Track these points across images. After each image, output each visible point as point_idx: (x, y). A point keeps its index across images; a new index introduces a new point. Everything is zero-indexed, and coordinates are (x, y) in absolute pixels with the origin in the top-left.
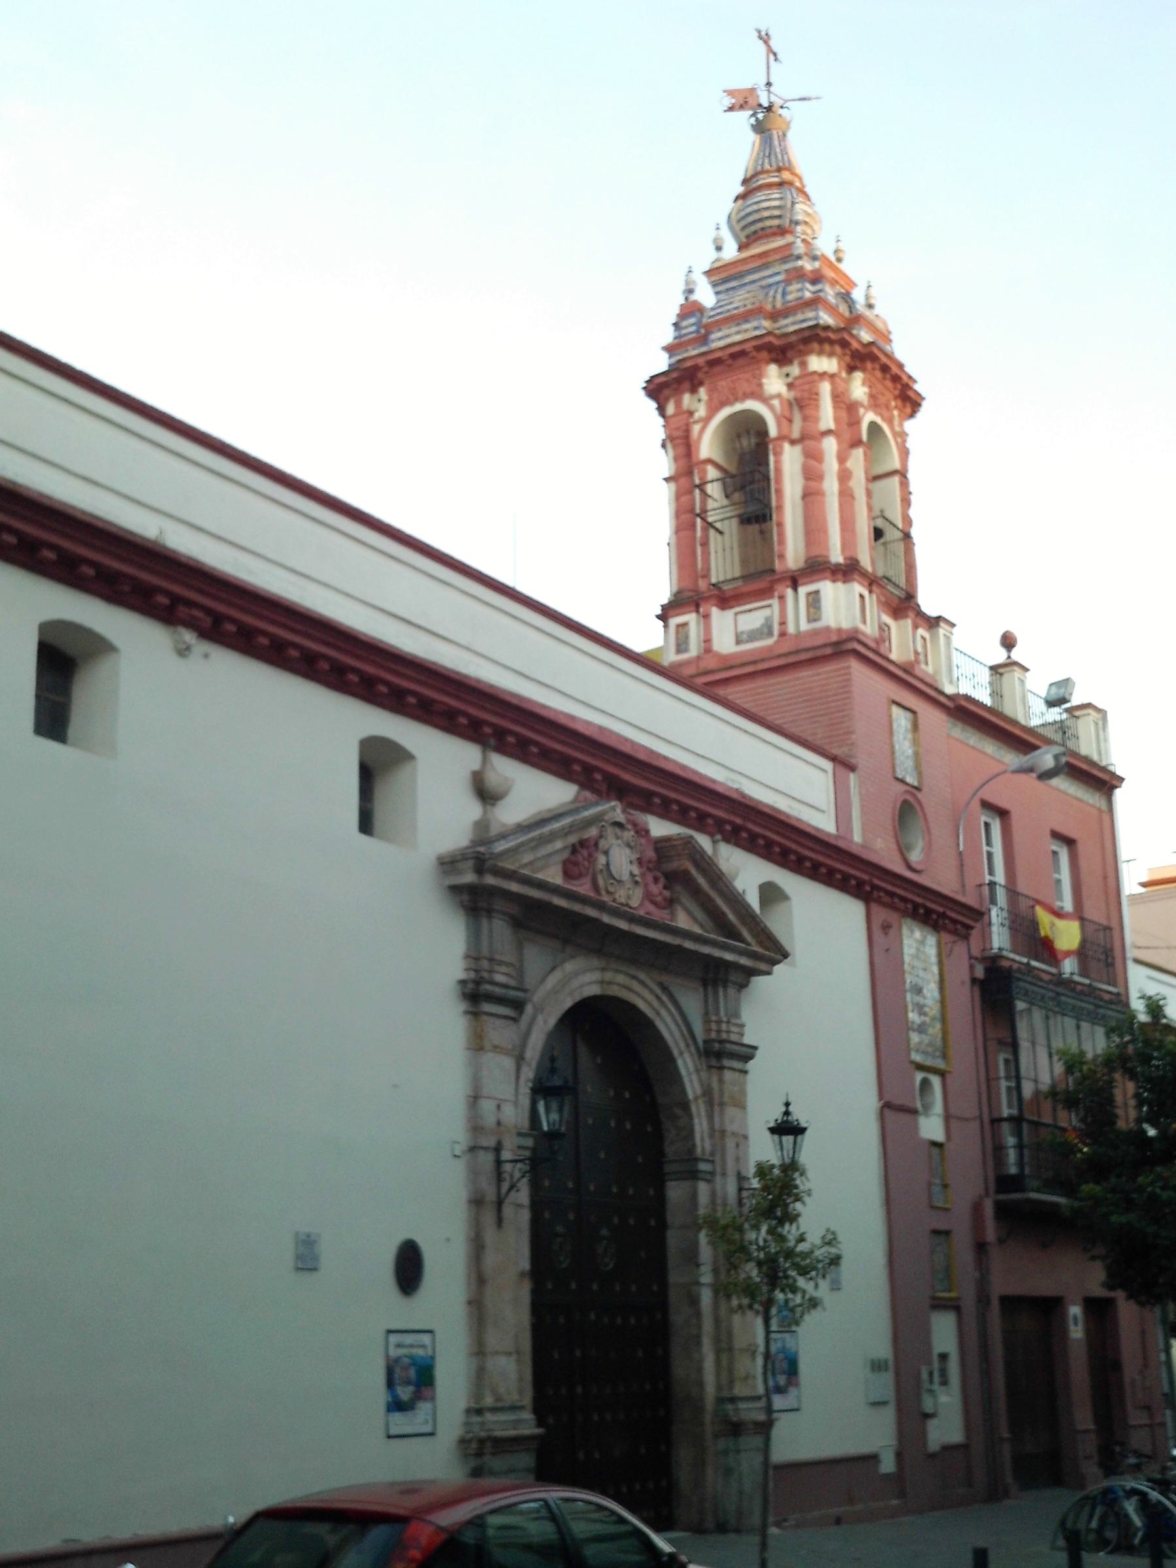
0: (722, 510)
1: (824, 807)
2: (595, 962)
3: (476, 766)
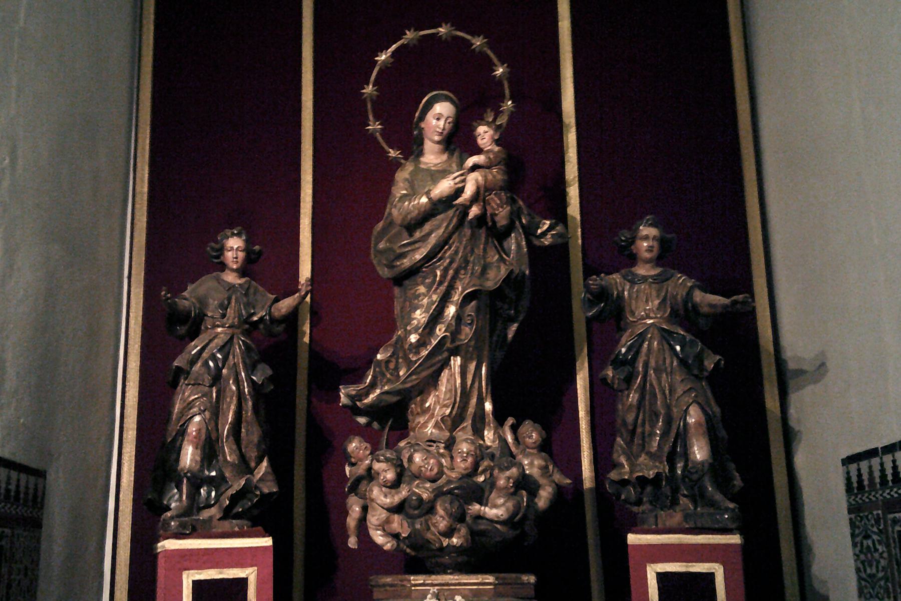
0: (31, 491)
1: (682, 497)
2: (304, 523)
3: (892, 458)
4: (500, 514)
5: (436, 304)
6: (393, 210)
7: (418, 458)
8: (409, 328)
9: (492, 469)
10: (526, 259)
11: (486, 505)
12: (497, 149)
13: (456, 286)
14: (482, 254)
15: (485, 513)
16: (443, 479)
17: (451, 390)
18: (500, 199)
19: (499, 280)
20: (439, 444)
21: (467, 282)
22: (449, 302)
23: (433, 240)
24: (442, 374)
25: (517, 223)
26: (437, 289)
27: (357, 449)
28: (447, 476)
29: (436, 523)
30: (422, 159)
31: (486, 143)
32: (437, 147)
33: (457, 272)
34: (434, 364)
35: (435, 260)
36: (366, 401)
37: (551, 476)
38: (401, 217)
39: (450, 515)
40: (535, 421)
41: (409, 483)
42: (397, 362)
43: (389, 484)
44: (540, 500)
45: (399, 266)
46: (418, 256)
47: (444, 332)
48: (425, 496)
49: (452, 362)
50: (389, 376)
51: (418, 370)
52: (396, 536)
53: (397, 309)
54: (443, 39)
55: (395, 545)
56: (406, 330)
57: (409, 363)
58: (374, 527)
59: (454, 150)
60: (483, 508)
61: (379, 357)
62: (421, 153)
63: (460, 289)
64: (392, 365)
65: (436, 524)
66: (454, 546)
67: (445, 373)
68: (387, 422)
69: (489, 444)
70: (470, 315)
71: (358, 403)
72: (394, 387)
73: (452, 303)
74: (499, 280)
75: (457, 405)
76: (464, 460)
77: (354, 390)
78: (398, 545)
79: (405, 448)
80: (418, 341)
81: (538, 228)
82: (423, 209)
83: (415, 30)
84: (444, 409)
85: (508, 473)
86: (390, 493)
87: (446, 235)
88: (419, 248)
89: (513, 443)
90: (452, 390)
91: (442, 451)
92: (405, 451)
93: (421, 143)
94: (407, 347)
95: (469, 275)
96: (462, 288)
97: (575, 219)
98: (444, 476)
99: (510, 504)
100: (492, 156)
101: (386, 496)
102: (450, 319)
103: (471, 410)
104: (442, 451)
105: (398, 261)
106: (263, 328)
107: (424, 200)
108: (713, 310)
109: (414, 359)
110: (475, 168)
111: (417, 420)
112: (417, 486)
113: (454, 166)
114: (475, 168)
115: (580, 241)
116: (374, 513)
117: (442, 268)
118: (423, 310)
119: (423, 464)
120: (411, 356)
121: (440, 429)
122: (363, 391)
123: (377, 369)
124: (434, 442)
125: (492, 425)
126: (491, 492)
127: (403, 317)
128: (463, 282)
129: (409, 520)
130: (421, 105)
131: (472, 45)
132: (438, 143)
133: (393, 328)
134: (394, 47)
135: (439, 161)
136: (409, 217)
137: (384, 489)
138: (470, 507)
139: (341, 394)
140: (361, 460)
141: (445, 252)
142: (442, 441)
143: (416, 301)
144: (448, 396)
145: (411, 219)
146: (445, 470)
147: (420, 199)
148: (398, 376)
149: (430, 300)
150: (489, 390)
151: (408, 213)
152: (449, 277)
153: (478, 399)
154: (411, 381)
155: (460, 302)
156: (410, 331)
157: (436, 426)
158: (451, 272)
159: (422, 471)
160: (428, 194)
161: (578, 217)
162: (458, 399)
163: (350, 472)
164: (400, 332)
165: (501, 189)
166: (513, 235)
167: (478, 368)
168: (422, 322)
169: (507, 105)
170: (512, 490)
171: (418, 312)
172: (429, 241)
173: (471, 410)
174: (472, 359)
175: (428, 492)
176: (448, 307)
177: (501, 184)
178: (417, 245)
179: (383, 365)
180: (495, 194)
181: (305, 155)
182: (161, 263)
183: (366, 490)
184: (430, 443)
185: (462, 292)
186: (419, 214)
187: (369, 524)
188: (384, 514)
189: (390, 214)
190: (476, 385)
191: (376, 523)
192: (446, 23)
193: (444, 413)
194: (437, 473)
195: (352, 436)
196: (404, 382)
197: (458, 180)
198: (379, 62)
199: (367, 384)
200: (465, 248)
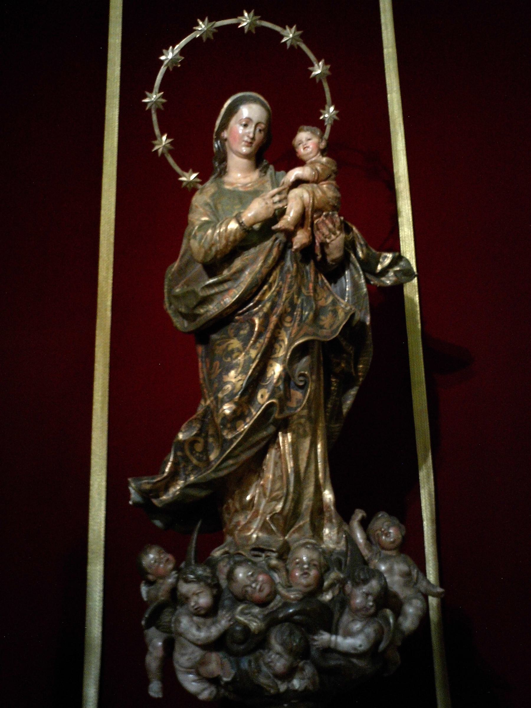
4: (358, 645)
5: (257, 361)
6: (192, 241)
7: (241, 573)
8: (220, 395)
9: (342, 582)
10: (366, 303)
11: (336, 633)
12: (324, 160)
13: (280, 338)
14: (312, 294)
15: (336, 643)
16: (277, 602)
17: (281, 477)
18: (333, 223)
19: (338, 327)
20: (269, 554)
21: (294, 331)
22: (273, 359)
23: (247, 278)
24: (268, 456)
25: (353, 256)
26: (255, 342)
27: (155, 562)
28: (282, 596)
29: (271, 662)
30: (226, 179)
31: (311, 153)
32: (244, 162)
33: (281, 319)
34: (258, 443)
35: (251, 304)
36: (164, 497)
37: (416, 584)
38: (203, 250)
39: (290, 651)
40: (391, 513)
41: (232, 608)
42: (206, 443)
43: (203, 612)
44: (406, 618)
45: (297, 594)
46: (229, 300)
47: (269, 398)
48: (254, 625)
49: (281, 439)
50: (195, 461)
51: (237, 452)
52: (214, 681)
53: (202, 374)
54: (246, 31)
55: (215, 692)
56: (216, 398)
57: (223, 443)
58: (185, 670)
59: (267, 167)
60: (333, 638)
61: (181, 436)
62: (224, 171)
63: (286, 343)
64: (199, 447)
65: (272, 664)
66: (296, 691)
67: (271, 454)
68: (196, 524)
69: (332, 546)
70: (303, 375)
71: (155, 501)
72: (204, 477)
73: (276, 360)
74: (338, 327)
75: (290, 497)
76: (305, 574)
77: (148, 483)
78: (218, 691)
79: (222, 559)
80: (234, 412)
81: (378, 262)
82: (232, 238)
83: (210, 21)
84: (274, 503)
85: (365, 589)
86: (204, 624)
87: (265, 271)
88: (227, 290)
89: (366, 545)
90: (282, 477)
91: (274, 562)
92: (222, 564)
93: (224, 159)
94: (218, 421)
95: (296, 323)
96: (289, 340)
97: (412, 300)
98: (278, 597)
99: (370, 630)
100: (319, 168)
101: (199, 629)
102: (275, 381)
103: (307, 503)
104: (274, 562)
105: (202, 308)
106: (326, 187)
107: (233, 225)
108: (356, 652)
109: (230, 437)
110: (298, 183)
111: (235, 520)
112: (242, 613)
113: (268, 185)
114: (298, 183)
115: (419, 326)
116: (183, 652)
117: (261, 314)
118: (240, 369)
119: (249, 582)
120: (225, 433)
121: (270, 532)
122: (159, 484)
123: (179, 453)
124: (263, 550)
125: (334, 521)
126: (341, 614)
127: (211, 382)
128: (289, 332)
129: (232, 659)
130: (223, 111)
131: (282, 37)
132: (247, 156)
133: (199, 396)
134: (183, 42)
135: (248, 180)
136: (214, 249)
137: (195, 618)
138: (316, 637)
139: (130, 488)
140: (164, 577)
141: (264, 294)
142: (274, 549)
143: (229, 359)
144: (278, 485)
145: (217, 252)
146: (280, 589)
147: (228, 224)
148: (208, 462)
149: (247, 357)
150: (328, 474)
151: (213, 245)
152: (271, 326)
153: (257, 453)
154: (226, 468)
155: (288, 357)
156: (223, 398)
157: (264, 527)
158: (274, 319)
159: (246, 591)
160: (238, 218)
161: (417, 299)
162: (291, 489)
163: (148, 592)
164: (208, 402)
165: (334, 208)
166: (346, 273)
167: (313, 445)
168: (239, 385)
169: (328, 112)
170: (372, 611)
171: (232, 373)
172: (242, 279)
173: (307, 503)
174: (305, 436)
175: (257, 620)
176: (271, 365)
177: (333, 202)
178: (226, 286)
179: (186, 447)
180: (326, 216)
181: (102, 417)
182: (101, 326)
183: (170, 622)
184: (256, 553)
185: (290, 344)
186: (226, 246)
187: (177, 666)
188: (198, 653)
189: (189, 248)
190: (312, 468)
191: (187, 664)
192: (337, 115)
193: (274, 510)
194: (268, 595)
195: (404, 533)
196: (217, 470)
197: (277, 198)
198: (166, 63)
199: (165, 475)
200: (290, 287)
